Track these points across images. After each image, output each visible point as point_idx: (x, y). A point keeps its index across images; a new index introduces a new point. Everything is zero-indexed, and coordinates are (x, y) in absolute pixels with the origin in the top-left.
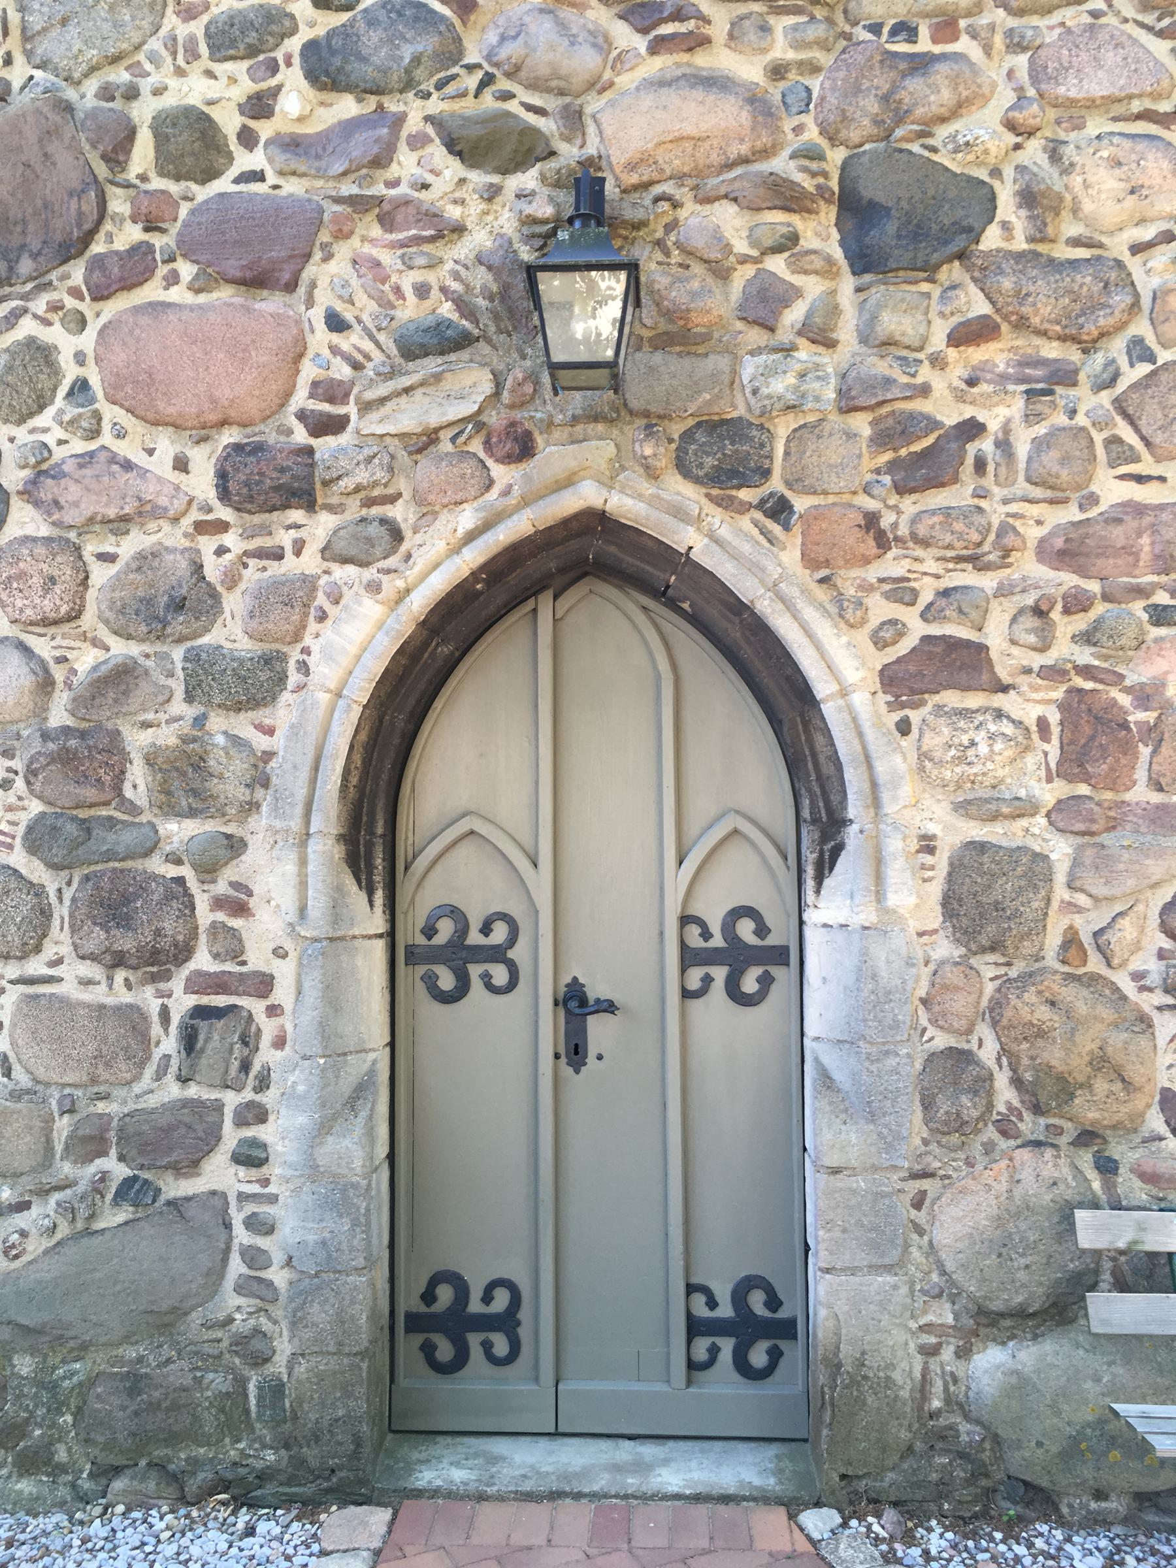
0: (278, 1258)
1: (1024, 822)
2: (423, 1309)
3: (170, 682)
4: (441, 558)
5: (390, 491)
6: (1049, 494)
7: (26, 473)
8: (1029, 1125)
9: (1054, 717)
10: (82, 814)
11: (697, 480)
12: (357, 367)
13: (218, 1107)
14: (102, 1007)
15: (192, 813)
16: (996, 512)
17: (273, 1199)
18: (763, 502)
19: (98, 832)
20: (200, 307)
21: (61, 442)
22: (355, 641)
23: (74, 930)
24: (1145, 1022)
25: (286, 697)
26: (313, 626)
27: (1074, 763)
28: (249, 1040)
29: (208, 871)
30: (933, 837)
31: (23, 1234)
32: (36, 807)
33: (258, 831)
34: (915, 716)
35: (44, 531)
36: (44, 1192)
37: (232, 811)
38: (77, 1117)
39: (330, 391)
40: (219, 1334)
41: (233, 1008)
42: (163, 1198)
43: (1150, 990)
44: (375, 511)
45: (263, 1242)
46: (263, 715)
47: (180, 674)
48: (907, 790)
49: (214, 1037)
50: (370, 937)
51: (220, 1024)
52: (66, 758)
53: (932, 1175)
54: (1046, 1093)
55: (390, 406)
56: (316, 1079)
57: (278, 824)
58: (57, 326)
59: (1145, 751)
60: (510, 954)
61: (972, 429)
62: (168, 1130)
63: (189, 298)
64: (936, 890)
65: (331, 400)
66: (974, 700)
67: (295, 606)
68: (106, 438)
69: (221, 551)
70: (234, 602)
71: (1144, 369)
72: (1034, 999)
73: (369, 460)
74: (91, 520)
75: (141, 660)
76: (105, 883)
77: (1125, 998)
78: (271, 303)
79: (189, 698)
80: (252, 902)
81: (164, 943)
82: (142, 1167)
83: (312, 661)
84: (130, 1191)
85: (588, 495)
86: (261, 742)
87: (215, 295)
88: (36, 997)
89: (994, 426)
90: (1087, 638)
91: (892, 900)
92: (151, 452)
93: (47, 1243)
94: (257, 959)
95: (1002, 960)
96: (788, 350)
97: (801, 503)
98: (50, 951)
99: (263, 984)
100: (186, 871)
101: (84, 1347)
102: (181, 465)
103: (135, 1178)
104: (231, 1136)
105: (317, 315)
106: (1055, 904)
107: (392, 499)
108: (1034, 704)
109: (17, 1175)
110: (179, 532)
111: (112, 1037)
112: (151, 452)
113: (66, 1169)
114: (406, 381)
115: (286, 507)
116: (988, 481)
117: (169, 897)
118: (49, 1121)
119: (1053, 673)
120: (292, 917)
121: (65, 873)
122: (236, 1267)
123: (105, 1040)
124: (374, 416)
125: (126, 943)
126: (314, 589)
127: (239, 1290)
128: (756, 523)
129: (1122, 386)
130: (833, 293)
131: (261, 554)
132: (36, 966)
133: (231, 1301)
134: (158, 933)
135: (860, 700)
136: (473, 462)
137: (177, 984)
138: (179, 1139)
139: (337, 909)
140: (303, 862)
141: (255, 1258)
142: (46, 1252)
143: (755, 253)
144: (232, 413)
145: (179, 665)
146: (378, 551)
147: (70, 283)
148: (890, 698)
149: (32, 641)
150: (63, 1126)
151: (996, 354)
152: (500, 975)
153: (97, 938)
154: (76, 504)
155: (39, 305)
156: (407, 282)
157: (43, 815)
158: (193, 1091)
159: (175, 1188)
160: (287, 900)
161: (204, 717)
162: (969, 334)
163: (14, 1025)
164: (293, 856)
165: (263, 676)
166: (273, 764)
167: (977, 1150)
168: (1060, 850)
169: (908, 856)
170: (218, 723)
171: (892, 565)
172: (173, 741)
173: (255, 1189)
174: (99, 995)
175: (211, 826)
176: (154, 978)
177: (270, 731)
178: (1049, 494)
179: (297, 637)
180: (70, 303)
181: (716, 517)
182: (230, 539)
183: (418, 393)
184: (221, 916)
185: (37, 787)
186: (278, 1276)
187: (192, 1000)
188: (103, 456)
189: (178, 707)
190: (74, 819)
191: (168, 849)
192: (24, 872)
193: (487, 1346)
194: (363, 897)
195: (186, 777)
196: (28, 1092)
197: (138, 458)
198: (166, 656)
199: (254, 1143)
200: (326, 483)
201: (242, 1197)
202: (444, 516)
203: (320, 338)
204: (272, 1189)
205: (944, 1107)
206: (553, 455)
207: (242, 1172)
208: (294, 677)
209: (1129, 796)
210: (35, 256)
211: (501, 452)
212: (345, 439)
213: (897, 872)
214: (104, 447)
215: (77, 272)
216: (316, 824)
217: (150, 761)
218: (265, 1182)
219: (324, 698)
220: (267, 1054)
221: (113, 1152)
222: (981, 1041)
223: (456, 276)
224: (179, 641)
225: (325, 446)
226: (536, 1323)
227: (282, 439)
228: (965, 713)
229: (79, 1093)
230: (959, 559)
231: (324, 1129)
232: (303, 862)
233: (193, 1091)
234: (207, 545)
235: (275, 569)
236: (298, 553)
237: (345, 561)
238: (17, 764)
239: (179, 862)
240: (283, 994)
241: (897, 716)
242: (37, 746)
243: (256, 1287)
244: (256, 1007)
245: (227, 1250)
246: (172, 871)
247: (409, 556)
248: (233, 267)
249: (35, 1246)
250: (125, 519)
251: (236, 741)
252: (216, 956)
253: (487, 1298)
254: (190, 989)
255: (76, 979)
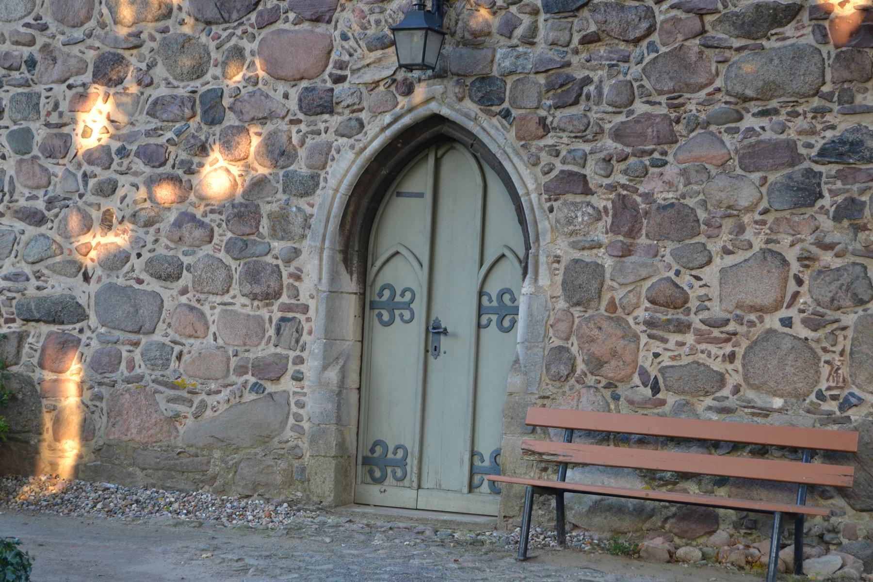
0: (305, 418)
1: (595, 251)
2: (369, 455)
3: (277, 185)
4: (375, 136)
5: (360, 107)
6: (614, 109)
7: (232, 100)
8: (591, 380)
9: (610, 205)
10: (245, 238)
11: (475, 102)
12: (351, 55)
13: (287, 357)
14: (249, 315)
15: (283, 239)
16: (593, 116)
17: (305, 395)
18: (500, 112)
19: (250, 245)
20: (296, 31)
21: (244, 87)
22: (344, 169)
23: (240, 284)
24: (637, 338)
25: (319, 192)
26: (330, 163)
27: (614, 229)
28: (299, 331)
29: (288, 262)
30: (559, 257)
31: (218, 402)
32: (229, 235)
33: (305, 246)
34: (556, 205)
35: (237, 123)
36: (226, 386)
37: (297, 238)
38: (238, 358)
39: (341, 65)
40: (284, 446)
41: (294, 318)
42: (266, 392)
43: (639, 324)
44: (355, 115)
45: (301, 411)
46: (309, 199)
47: (281, 182)
48: (549, 237)
49: (287, 329)
50: (350, 293)
51: (289, 324)
52: (239, 216)
53: (548, 397)
54: (596, 364)
55: (362, 71)
56: (322, 348)
57: (312, 244)
58: (245, 40)
59: (645, 222)
60: (412, 306)
61: (588, 81)
62: (269, 364)
63: (292, 28)
64: (559, 279)
65: (341, 69)
66: (579, 199)
67: (324, 156)
68: (260, 85)
69: (299, 131)
70: (302, 153)
71: (653, 55)
72: (593, 326)
73: (352, 94)
74: (253, 119)
75: (269, 177)
76: (251, 266)
77: (630, 327)
78: (321, 28)
79: (284, 192)
80: (303, 276)
81: (271, 291)
82: (260, 379)
83: (328, 177)
84: (257, 388)
85: (433, 107)
86: (308, 210)
87: (302, 25)
88: (226, 310)
89: (596, 79)
90: (625, 172)
91: (541, 282)
92: (276, 91)
93: (226, 406)
94: (303, 298)
95: (582, 309)
96: (515, 47)
97: (515, 113)
98: (232, 292)
99: (305, 309)
100: (280, 262)
101: (238, 449)
102: (286, 96)
103: (257, 383)
104: (291, 369)
105: (337, 34)
106: (605, 287)
107: (361, 110)
108: (602, 201)
109: (217, 379)
110: (284, 123)
111: (251, 328)
112: (276, 91)
113: (233, 378)
114: (368, 61)
115: (322, 113)
116: (591, 103)
117: (273, 272)
118: (229, 359)
119: (612, 188)
120: (316, 282)
121: (238, 262)
122: (291, 421)
123: (249, 329)
124: (356, 76)
125: (257, 290)
126: (331, 147)
127: (292, 429)
128: (498, 120)
129: (644, 63)
130: (536, 21)
131: (313, 133)
132: (227, 298)
133: (288, 434)
134: (269, 286)
135: (534, 196)
136: (391, 95)
137: (275, 308)
138: (269, 370)
139: (334, 278)
140: (321, 260)
141: (298, 418)
142: (226, 410)
143: (505, 5)
144: (305, 75)
145: (281, 178)
146: (354, 132)
147: (251, 22)
148: (547, 197)
149: (231, 168)
150: (234, 361)
151: (601, 50)
152: (407, 315)
153: (247, 288)
154: (248, 113)
155: (239, 32)
156: (372, 18)
157: (231, 239)
158: (279, 350)
159: (271, 388)
160: (314, 276)
161: (289, 199)
162: (587, 40)
163: (218, 321)
164: (317, 257)
165: (311, 183)
166: (313, 219)
167: (567, 388)
168: (609, 263)
169: (548, 263)
170: (295, 201)
171: (549, 140)
172: (278, 209)
173: (298, 390)
174: (248, 310)
175: (290, 244)
176: (267, 305)
177: (312, 206)
178: (614, 109)
179: (324, 167)
180: (250, 30)
181: (482, 117)
182: (303, 127)
183: (372, 66)
184: (291, 281)
185: (230, 227)
186: (306, 425)
187: (280, 314)
188: (258, 93)
189: (280, 195)
190: (242, 240)
191: (274, 252)
192: (224, 261)
193: (394, 473)
194: (348, 277)
195: (281, 224)
196: (222, 347)
197: (271, 93)
198: (277, 174)
199: (298, 372)
200: (337, 103)
201: (295, 393)
202: (379, 117)
203: (338, 42)
204: (305, 391)
205: (553, 369)
206: (420, 92)
207: (294, 383)
208: (322, 184)
209: (639, 241)
210: (238, 11)
211: (401, 91)
212: (346, 85)
213: (543, 270)
214: (259, 89)
215: (253, 16)
216: (327, 244)
217: (269, 216)
218: (303, 388)
219: (331, 192)
220: (305, 337)
221: (250, 373)
222: (572, 344)
223: (390, 16)
224: (282, 168)
225: (338, 88)
226: (412, 463)
227: (323, 85)
228: (574, 204)
229: (238, 348)
230: (576, 137)
231: (325, 368)
232: (321, 260)
233: (279, 350)
234: (294, 129)
235: (318, 139)
236: (326, 132)
237: (343, 136)
238: (223, 217)
239: (277, 258)
240: (311, 313)
241: (548, 204)
242: (230, 211)
243: (299, 430)
244: (302, 317)
245: (288, 414)
246: (275, 262)
247: (366, 134)
248: (308, 14)
249: (223, 407)
250: (265, 118)
251: (299, 209)
252: (289, 297)
253: (395, 453)
254: (280, 310)
255: (242, 304)
